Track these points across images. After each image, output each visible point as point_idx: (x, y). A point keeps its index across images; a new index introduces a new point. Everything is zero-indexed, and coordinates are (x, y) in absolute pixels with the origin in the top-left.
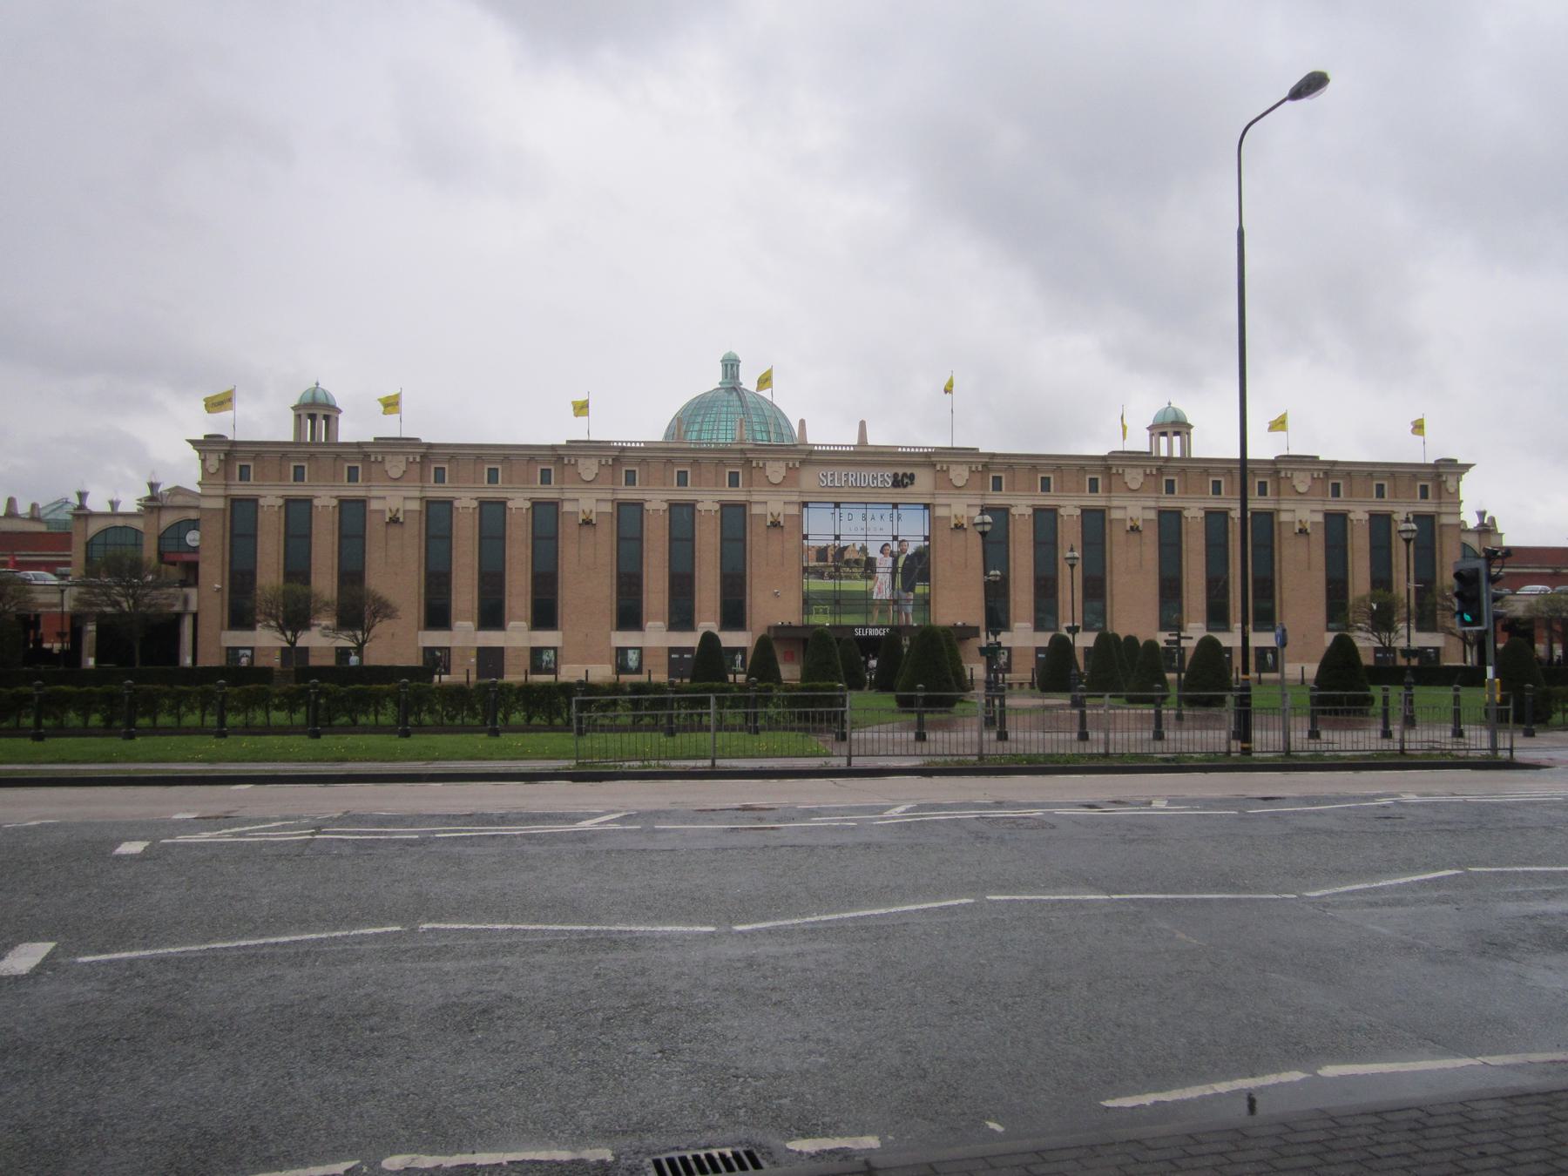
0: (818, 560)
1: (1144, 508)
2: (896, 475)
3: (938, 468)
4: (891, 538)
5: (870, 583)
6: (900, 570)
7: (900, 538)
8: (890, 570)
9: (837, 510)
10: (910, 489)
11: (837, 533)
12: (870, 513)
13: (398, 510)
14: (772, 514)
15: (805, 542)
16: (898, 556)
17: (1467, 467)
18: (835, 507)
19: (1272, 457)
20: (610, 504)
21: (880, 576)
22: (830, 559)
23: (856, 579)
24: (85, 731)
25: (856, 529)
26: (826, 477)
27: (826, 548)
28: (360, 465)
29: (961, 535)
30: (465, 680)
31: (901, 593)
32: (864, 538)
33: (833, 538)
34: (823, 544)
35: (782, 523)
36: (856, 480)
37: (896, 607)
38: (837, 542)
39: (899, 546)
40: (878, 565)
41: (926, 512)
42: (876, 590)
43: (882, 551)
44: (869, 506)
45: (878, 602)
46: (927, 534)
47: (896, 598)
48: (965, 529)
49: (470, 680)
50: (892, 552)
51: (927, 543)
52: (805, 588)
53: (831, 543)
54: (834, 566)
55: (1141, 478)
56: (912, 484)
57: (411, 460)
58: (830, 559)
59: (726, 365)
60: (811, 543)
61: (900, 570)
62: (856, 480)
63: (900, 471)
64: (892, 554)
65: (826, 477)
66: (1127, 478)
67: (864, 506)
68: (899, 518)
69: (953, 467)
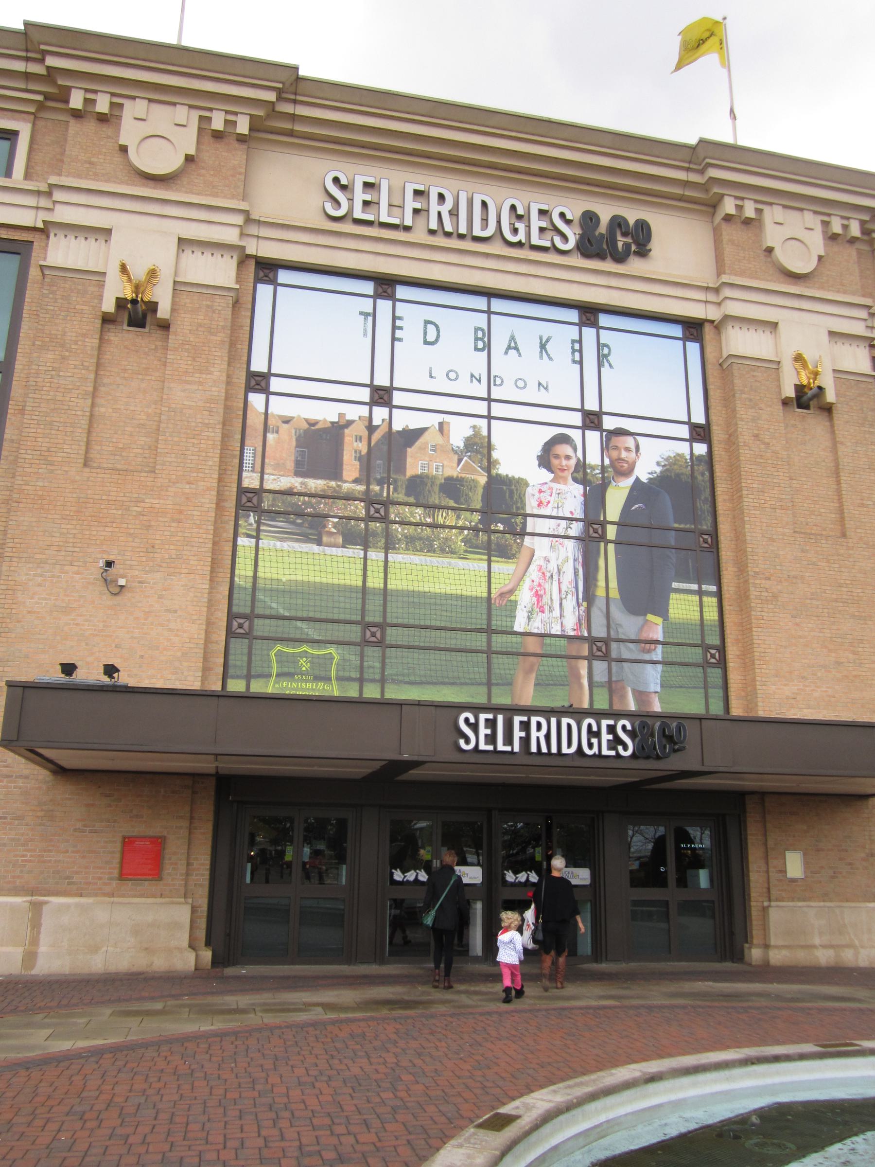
0: (301, 470)
2: (589, 219)
3: (729, 206)
4: (576, 419)
5: (503, 569)
6: (611, 532)
7: (609, 423)
8: (576, 529)
9: (384, 306)
10: (635, 265)
11: (382, 380)
12: (502, 328)
13: (153, 274)
14: (124, 269)
15: (257, 400)
16: (603, 487)
18: (377, 296)
19: (693, 141)
21: (541, 547)
22: (351, 469)
23: (447, 550)
25: (451, 375)
26: (475, 727)
27: (338, 429)
28: (25, 130)
29: (814, 422)
30: (697, 615)
31: (618, 614)
32: (481, 408)
33: (364, 394)
34: (328, 414)
35: (164, 311)
36: (548, 737)
37: (600, 667)
38: (380, 414)
39: (605, 447)
40: (531, 506)
41: (693, 348)
42: (524, 597)
43: (546, 459)
44: (498, 305)
45: (532, 645)
46: (699, 418)
47: (599, 631)
48: (828, 409)
49: (707, 616)
50: (582, 466)
51: (701, 449)
52: (244, 569)
53: (355, 413)
54: (369, 500)
55: (817, 243)
56: (643, 252)
57: (218, 124)
58: (351, 469)
60: (279, 407)
61: (611, 532)
62: (548, 737)
64: (581, 473)
65: (475, 727)
66: (773, 236)
67: (480, 303)
68: (602, 359)
69: (133, 109)
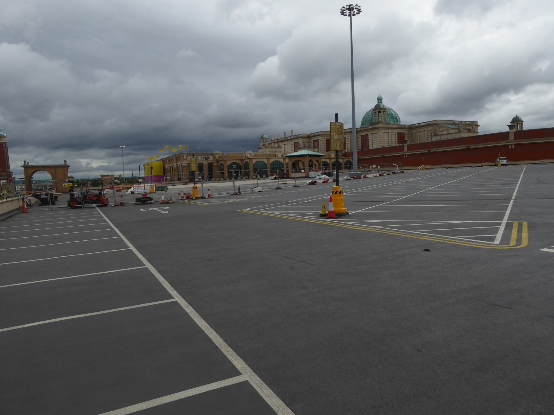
1: (384, 132)
2: (206, 157)
17: (508, 126)
20: (187, 164)
24: (512, 145)
59: (378, 100)
63: (207, 156)
